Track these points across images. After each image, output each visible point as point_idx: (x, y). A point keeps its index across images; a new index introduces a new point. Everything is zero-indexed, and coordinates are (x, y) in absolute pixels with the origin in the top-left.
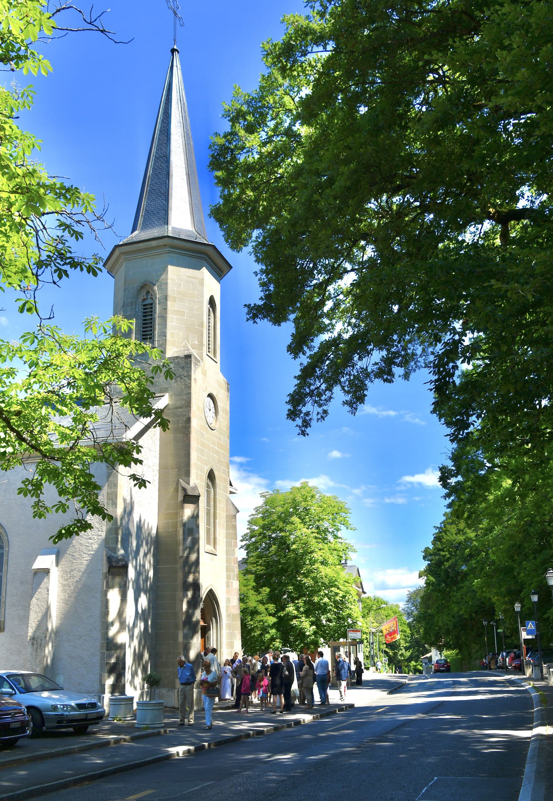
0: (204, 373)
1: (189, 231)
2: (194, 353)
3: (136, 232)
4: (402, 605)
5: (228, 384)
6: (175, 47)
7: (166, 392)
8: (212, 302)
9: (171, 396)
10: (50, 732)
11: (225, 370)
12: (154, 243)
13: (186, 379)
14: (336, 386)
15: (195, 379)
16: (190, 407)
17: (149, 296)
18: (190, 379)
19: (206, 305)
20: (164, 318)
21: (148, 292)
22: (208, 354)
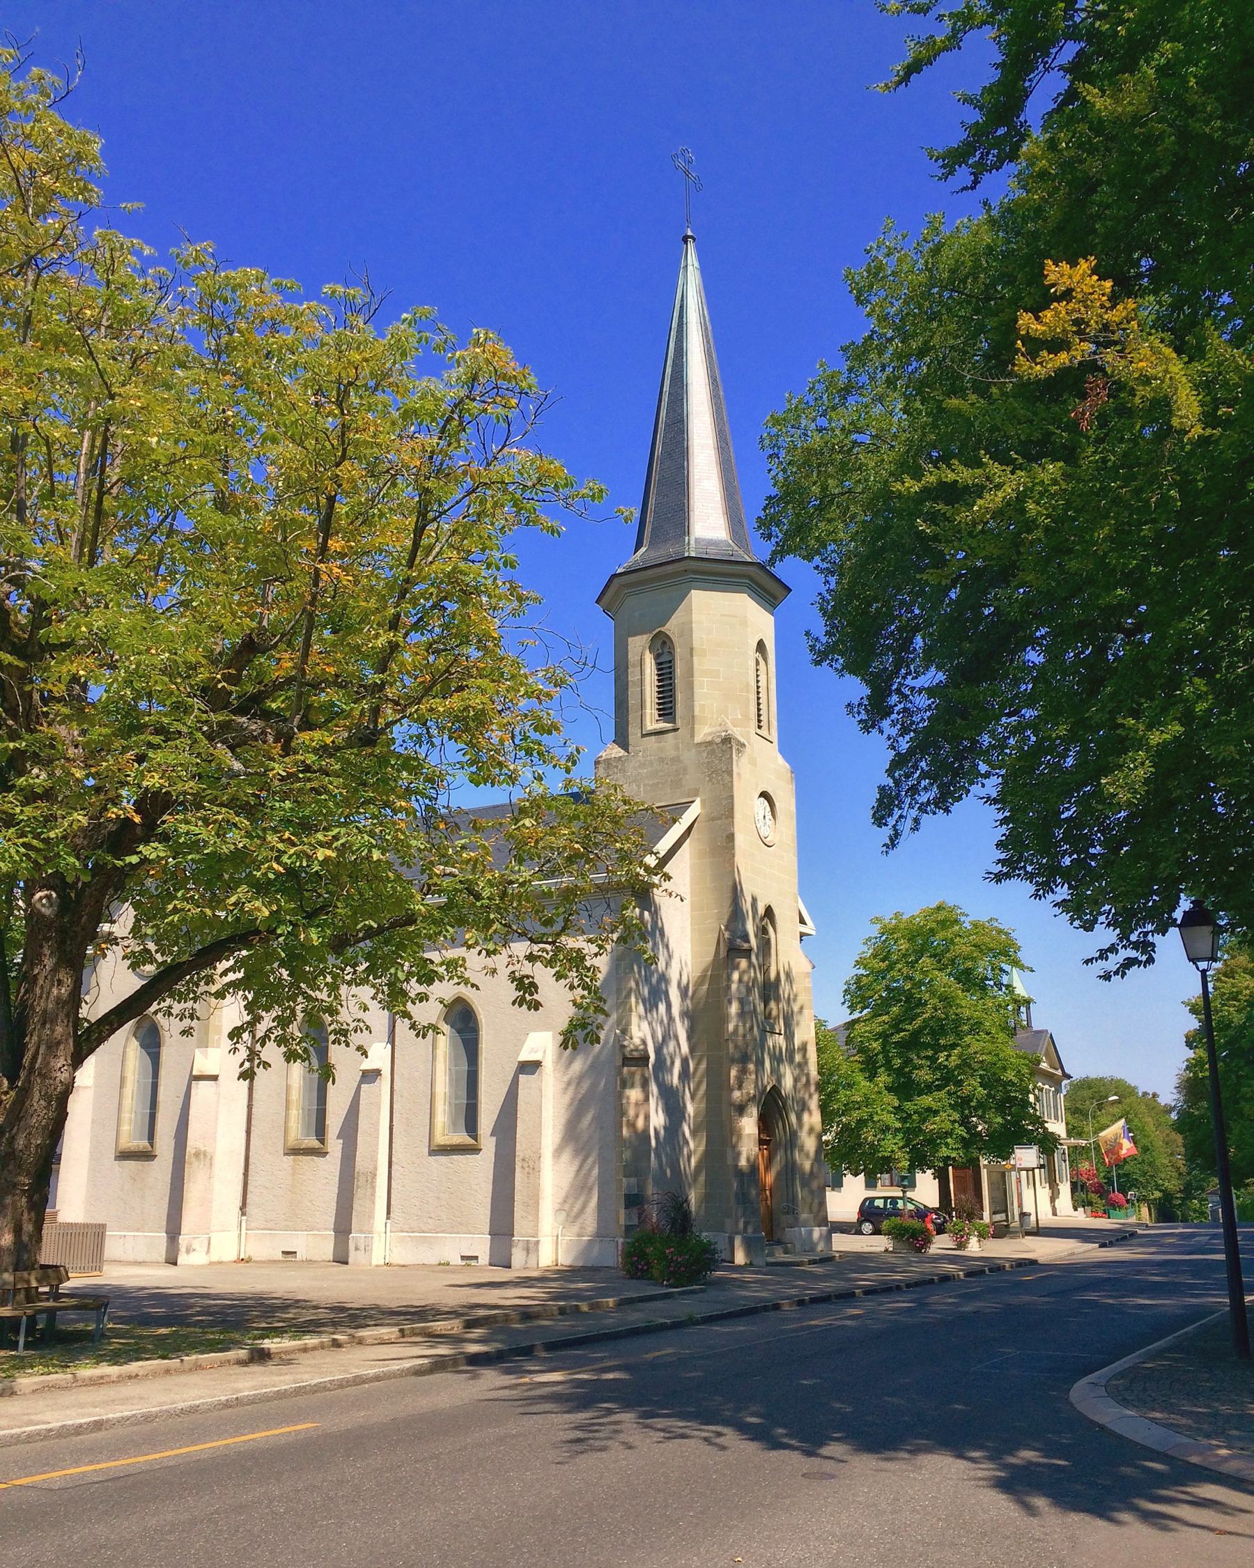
0: (753, 762)
1: (721, 541)
2: (737, 732)
3: (643, 550)
4: (1169, 1095)
5: (792, 772)
6: (689, 233)
7: (696, 795)
8: (761, 646)
9: (703, 802)
10: (723, 381)
11: (786, 749)
12: (670, 568)
13: (725, 775)
14: (913, 917)
15: (739, 774)
16: (733, 817)
17: (666, 650)
18: (731, 775)
19: (752, 654)
20: (690, 686)
21: (664, 643)
22: (759, 731)
